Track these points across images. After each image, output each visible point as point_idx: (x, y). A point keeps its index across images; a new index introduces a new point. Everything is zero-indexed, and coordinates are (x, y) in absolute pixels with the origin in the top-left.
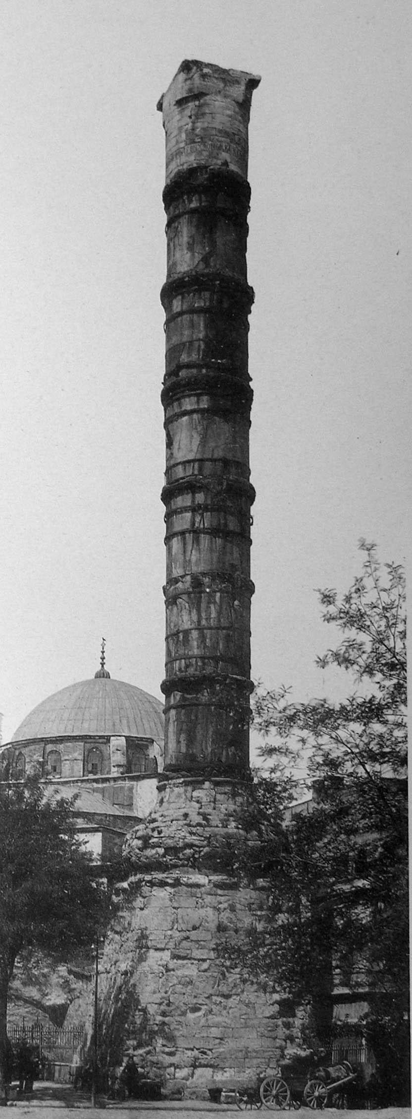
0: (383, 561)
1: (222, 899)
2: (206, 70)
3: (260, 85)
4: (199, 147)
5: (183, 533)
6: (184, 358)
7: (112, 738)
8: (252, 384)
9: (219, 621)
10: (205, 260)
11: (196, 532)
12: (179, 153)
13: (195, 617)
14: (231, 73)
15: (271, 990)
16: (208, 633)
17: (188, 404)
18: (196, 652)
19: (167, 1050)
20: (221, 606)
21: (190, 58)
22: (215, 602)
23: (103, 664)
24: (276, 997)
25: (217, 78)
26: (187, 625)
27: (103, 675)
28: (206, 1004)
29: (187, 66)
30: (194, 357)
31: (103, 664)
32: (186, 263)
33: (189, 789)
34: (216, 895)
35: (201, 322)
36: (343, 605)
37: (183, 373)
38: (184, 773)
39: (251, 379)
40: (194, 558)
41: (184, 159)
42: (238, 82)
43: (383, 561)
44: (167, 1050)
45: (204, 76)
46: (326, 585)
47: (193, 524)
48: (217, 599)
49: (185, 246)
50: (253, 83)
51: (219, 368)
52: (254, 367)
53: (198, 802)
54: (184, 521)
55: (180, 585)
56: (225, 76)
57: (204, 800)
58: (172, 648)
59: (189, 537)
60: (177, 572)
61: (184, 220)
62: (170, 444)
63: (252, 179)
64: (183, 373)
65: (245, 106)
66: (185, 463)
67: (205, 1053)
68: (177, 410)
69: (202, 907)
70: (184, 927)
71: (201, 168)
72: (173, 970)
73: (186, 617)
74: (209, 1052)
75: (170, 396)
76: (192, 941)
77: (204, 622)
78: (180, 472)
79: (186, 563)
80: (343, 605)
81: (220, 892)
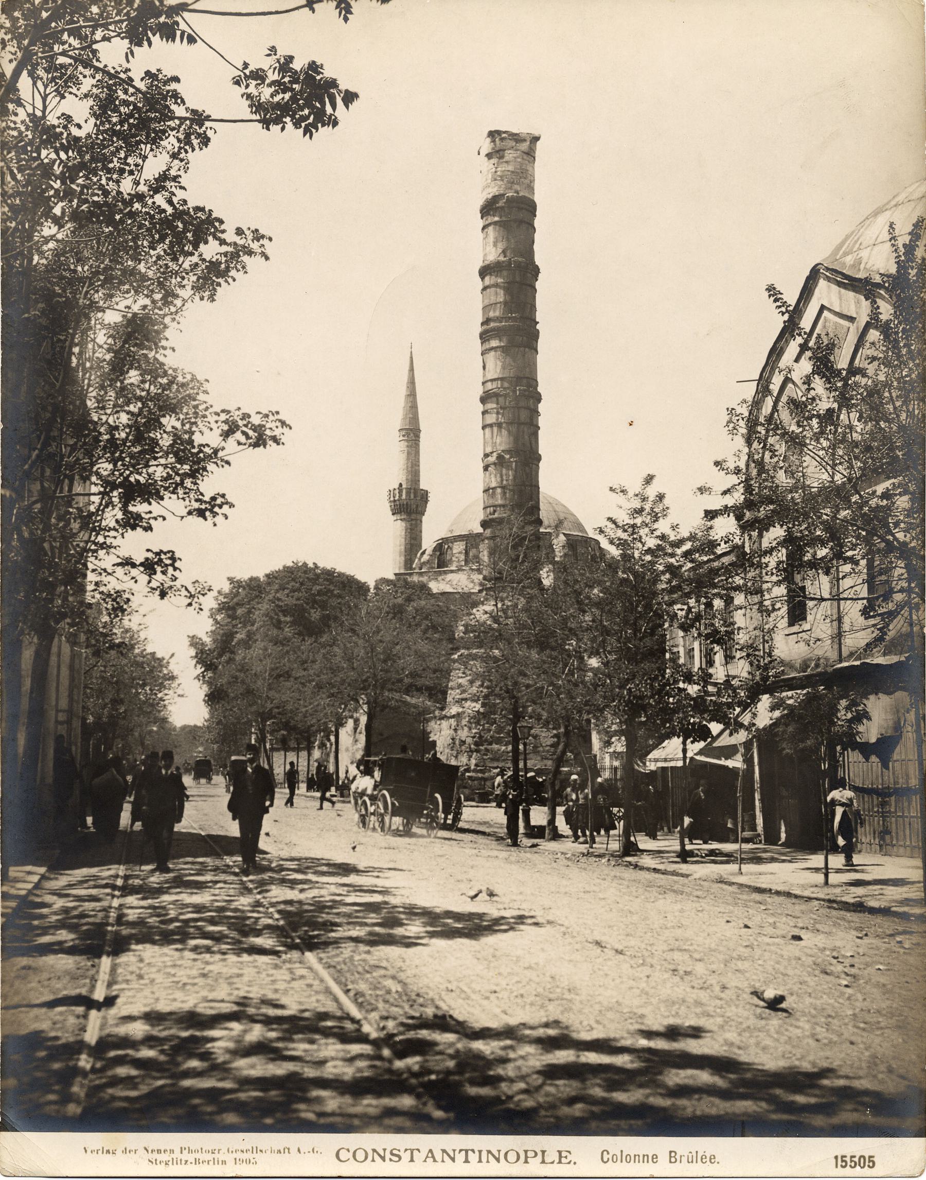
0: (155, 200)
2: (504, 135)
4: (499, 183)
5: (491, 426)
6: (491, 314)
7: (533, 823)
10: (504, 252)
11: (499, 425)
12: (488, 186)
13: (499, 479)
17: (494, 343)
18: (500, 502)
26: (493, 485)
29: (492, 134)
30: (497, 314)
32: (493, 255)
37: (492, 325)
40: (498, 441)
41: (490, 190)
42: (525, 140)
43: (155, 200)
45: (502, 139)
47: (497, 419)
49: (492, 244)
50: (537, 139)
51: (514, 319)
54: (491, 419)
55: (490, 458)
56: (516, 138)
59: (495, 429)
60: (489, 450)
61: (491, 228)
63: (537, 198)
64: (492, 325)
65: (530, 154)
66: (492, 380)
68: (488, 347)
71: (501, 196)
72: (115, 548)
73: (493, 479)
75: (484, 337)
76: (186, 968)
77: (505, 482)
78: (489, 386)
79: (494, 444)
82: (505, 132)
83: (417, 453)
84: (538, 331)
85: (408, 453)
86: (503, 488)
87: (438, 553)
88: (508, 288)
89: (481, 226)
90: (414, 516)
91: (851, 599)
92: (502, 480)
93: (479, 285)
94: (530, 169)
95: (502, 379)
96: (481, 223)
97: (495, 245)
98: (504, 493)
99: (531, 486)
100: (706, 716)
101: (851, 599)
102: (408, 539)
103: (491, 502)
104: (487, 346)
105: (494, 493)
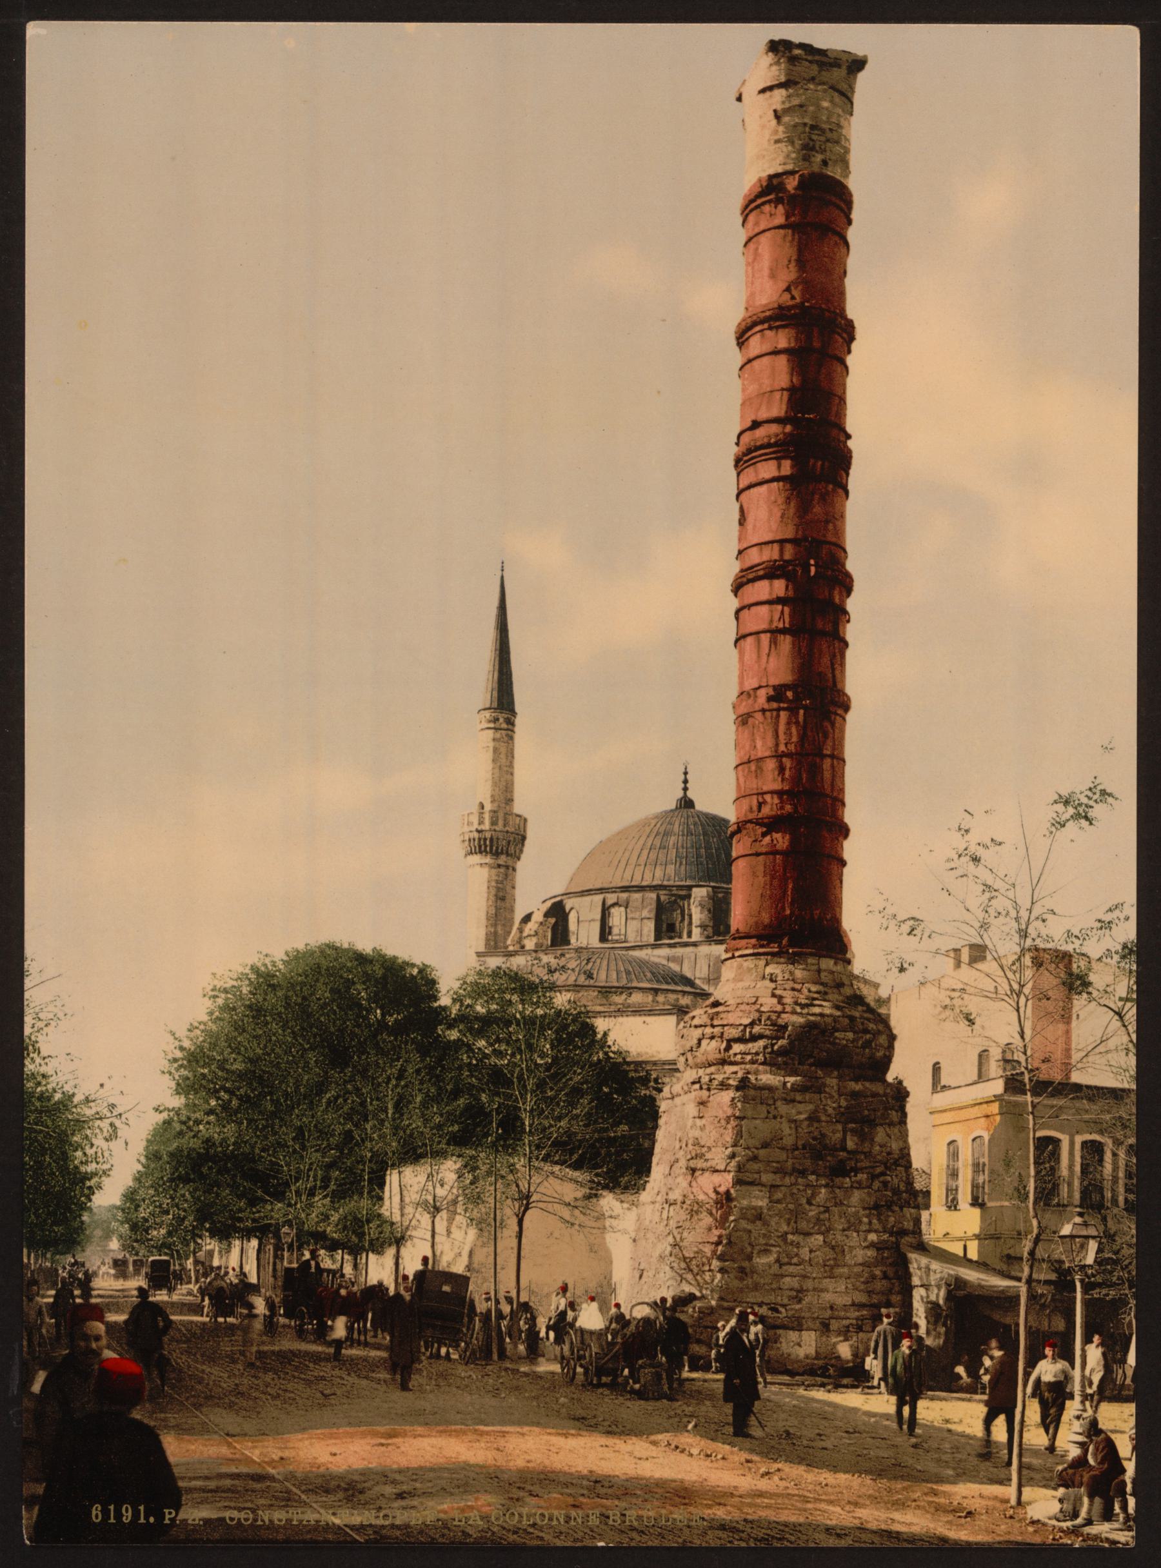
1: (801, 1107)
2: (797, 52)
3: (867, 67)
8: (850, 444)
9: (802, 745)
13: (770, 742)
14: (829, 54)
15: (867, 1227)
16: (787, 762)
19: (726, 1304)
20: (805, 727)
21: (777, 38)
22: (797, 723)
23: (685, 789)
24: (873, 1237)
25: (810, 62)
27: (686, 803)
28: (779, 1246)
31: (685, 789)
32: (769, 294)
33: (762, 963)
34: (793, 1101)
35: (782, 361)
36: (954, 1154)
38: (753, 941)
39: (849, 437)
44: (726, 1304)
46: (215, 971)
48: (801, 719)
49: (766, 272)
52: (852, 423)
53: (772, 980)
57: (780, 978)
58: (742, 780)
61: (764, 239)
62: (742, 521)
67: (777, 1311)
69: (775, 1117)
70: (752, 1142)
74: (782, 1310)
80: (954, 1154)
81: (799, 1097)
82: (802, 46)
83: (511, 754)
84: (850, 451)
85: (495, 750)
86: (779, 756)
87: (553, 920)
88: (798, 356)
89: (744, 240)
90: (502, 859)
91: (433, 1236)
92: (777, 745)
93: (736, 357)
94: (843, 122)
95: (782, 542)
96: (742, 235)
97: (773, 276)
98: (781, 769)
99: (832, 756)
100: (720, 1325)
101: (433, 1236)
102: (492, 898)
103: (753, 784)
104: (749, 476)
105: (759, 769)
